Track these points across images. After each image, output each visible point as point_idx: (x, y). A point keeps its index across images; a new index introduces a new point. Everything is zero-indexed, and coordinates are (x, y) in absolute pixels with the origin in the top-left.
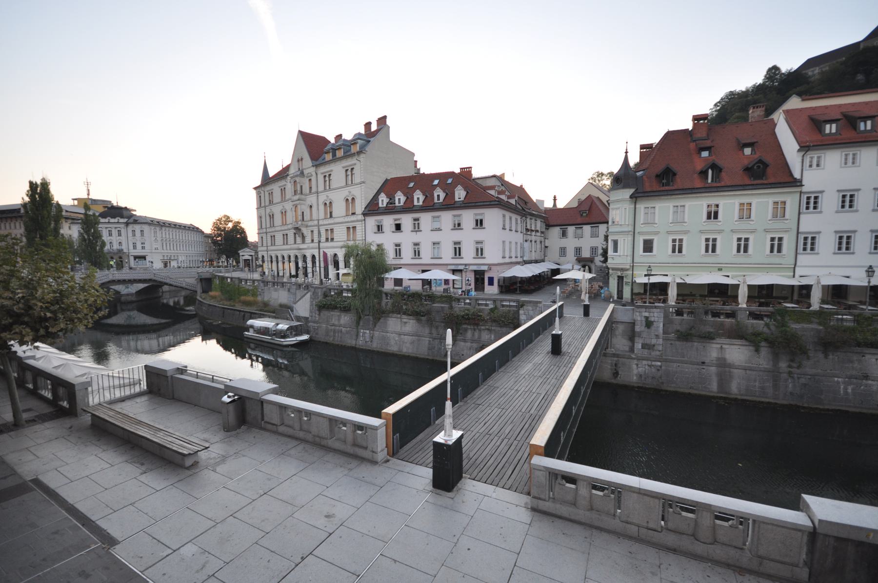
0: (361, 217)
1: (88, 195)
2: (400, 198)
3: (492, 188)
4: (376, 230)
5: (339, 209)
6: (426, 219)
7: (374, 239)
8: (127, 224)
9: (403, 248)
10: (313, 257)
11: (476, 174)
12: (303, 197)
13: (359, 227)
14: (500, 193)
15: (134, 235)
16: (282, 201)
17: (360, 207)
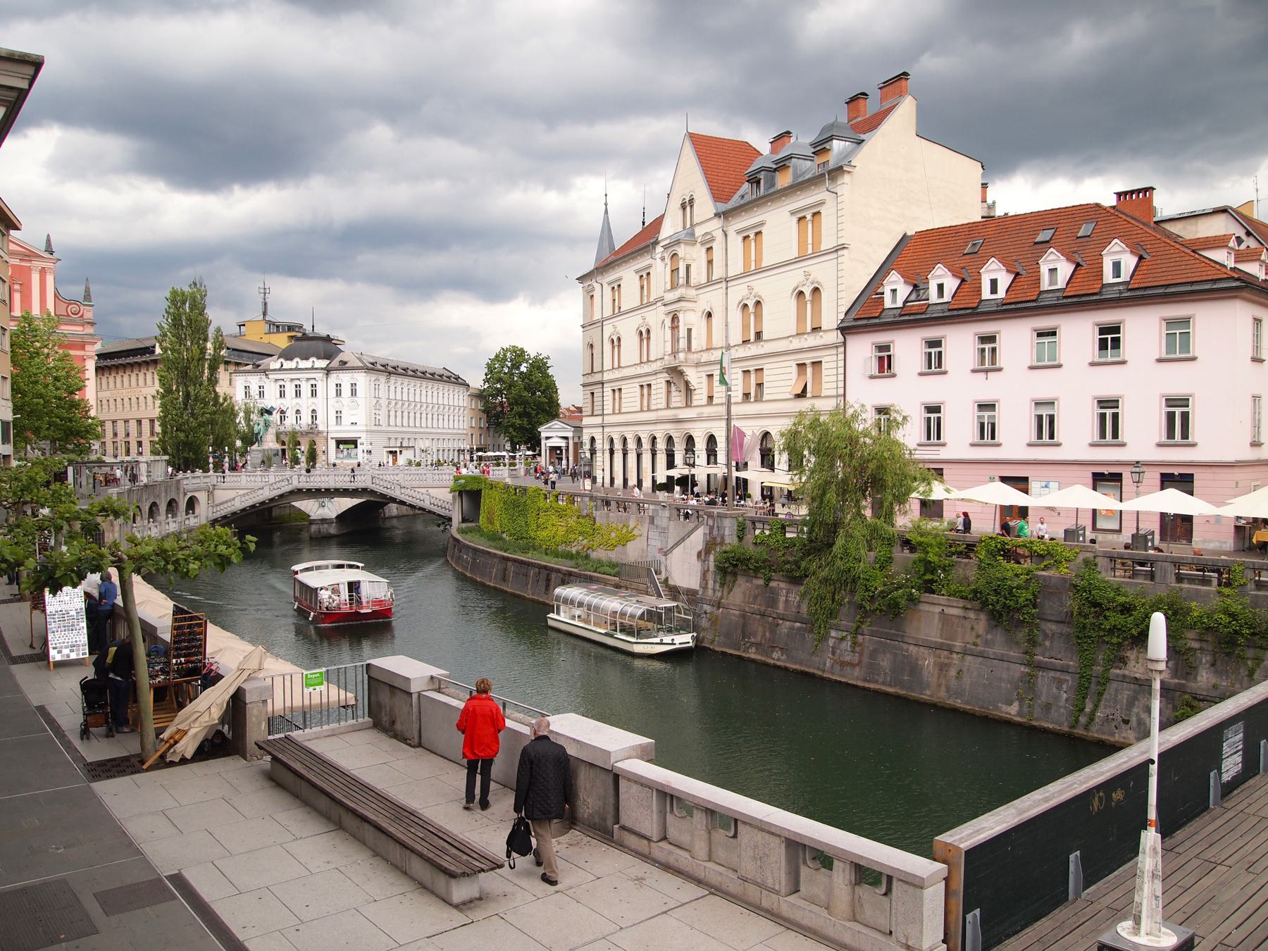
0: (835, 337)
1: (265, 314)
2: (995, 277)
3: (1218, 242)
4: (875, 371)
5: (780, 319)
6: (1016, 338)
7: (865, 395)
8: (328, 371)
9: (947, 416)
10: (711, 440)
11: (909, 234)
12: (691, 293)
13: (830, 362)
14: (1240, 257)
15: (339, 393)
16: (642, 306)
17: (832, 314)
